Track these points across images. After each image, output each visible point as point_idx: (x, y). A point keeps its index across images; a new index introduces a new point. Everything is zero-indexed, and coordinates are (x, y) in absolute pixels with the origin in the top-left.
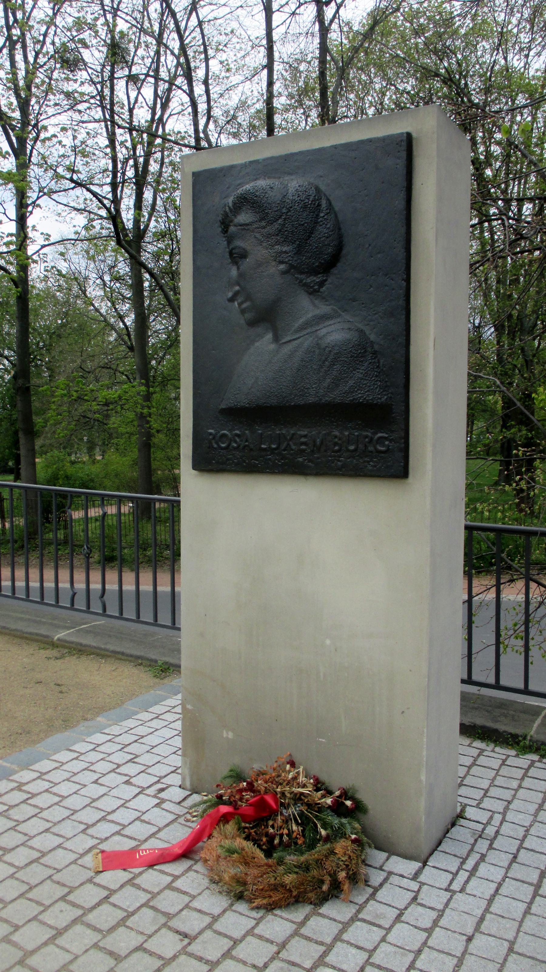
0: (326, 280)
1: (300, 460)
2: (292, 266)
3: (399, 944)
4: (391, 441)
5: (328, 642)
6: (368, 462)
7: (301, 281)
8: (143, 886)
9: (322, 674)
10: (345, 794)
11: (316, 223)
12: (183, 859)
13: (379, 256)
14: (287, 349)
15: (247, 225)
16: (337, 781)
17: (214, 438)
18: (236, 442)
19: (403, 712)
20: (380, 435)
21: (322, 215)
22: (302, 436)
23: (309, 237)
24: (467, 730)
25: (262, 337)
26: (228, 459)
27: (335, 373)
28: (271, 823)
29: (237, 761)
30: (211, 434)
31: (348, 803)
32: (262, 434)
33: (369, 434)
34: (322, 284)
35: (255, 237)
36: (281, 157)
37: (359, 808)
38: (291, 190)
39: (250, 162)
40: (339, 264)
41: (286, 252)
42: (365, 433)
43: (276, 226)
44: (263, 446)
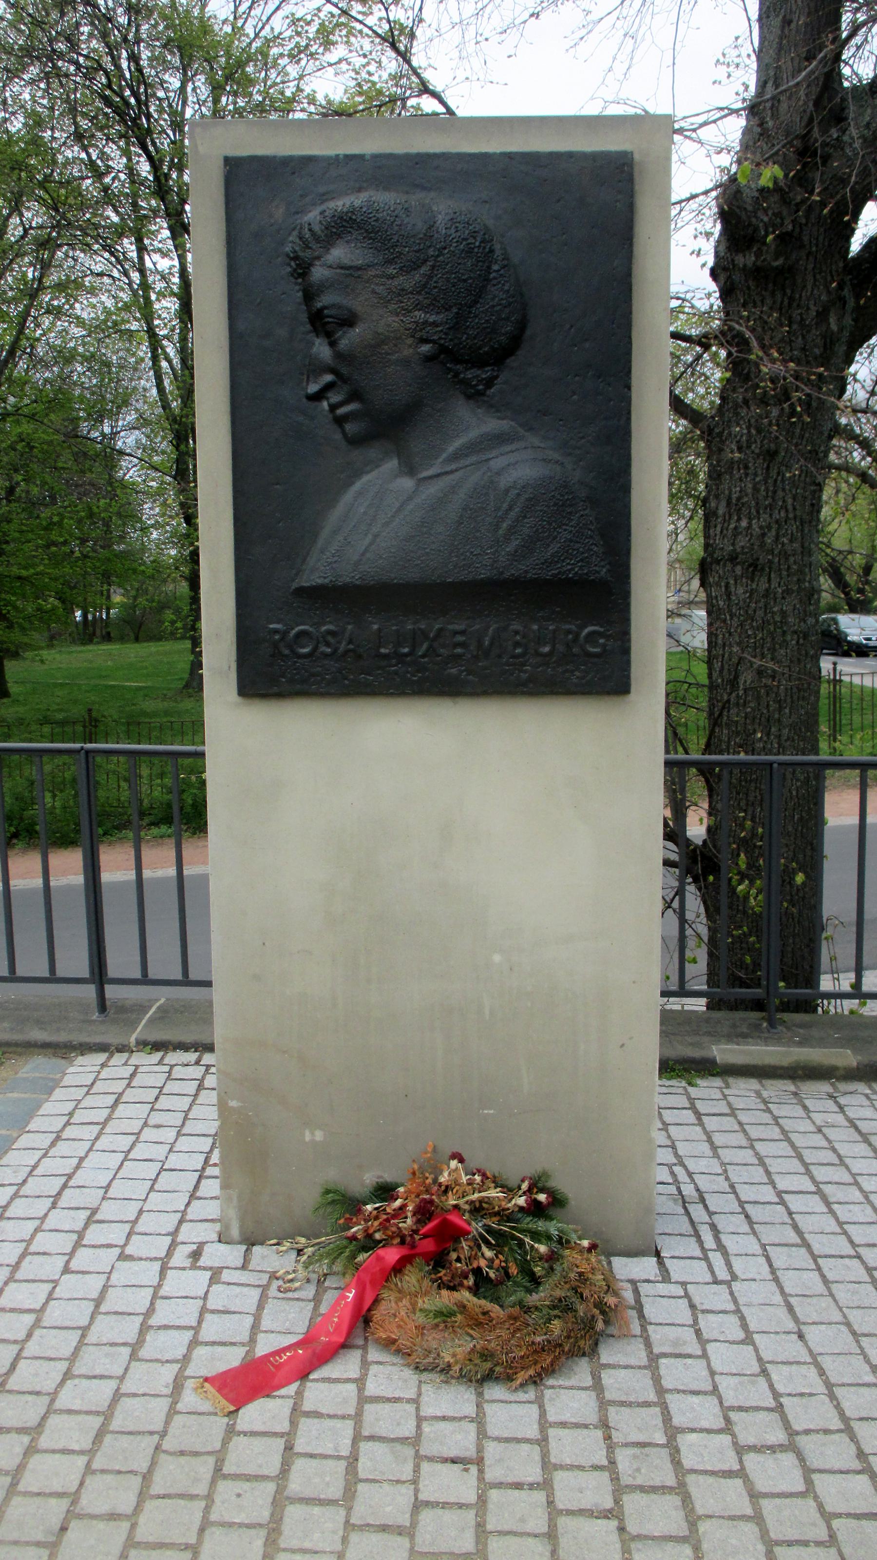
0: (497, 377)
1: (454, 671)
2: (443, 349)
3: (735, 1371)
4: (608, 637)
5: (497, 958)
6: (573, 671)
7: (456, 375)
8: (324, 1411)
9: (487, 1012)
10: (536, 1185)
11: (487, 280)
12: (341, 1351)
13: (587, 345)
14: (433, 489)
15: (358, 268)
16: (517, 1166)
17: (282, 639)
18: (328, 644)
19: (622, 1046)
20: (591, 628)
21: (495, 267)
22: (456, 633)
23: (476, 302)
25: (378, 466)
26: (313, 675)
27: (526, 531)
28: (454, 1256)
29: (332, 1174)
30: (276, 631)
32: (379, 630)
33: (573, 627)
34: (489, 383)
35: (374, 292)
36: (408, 157)
37: (557, 1201)
38: (441, 220)
39: (346, 156)
40: (519, 353)
41: (434, 324)
42: (567, 627)
43: (417, 277)
44: (383, 650)
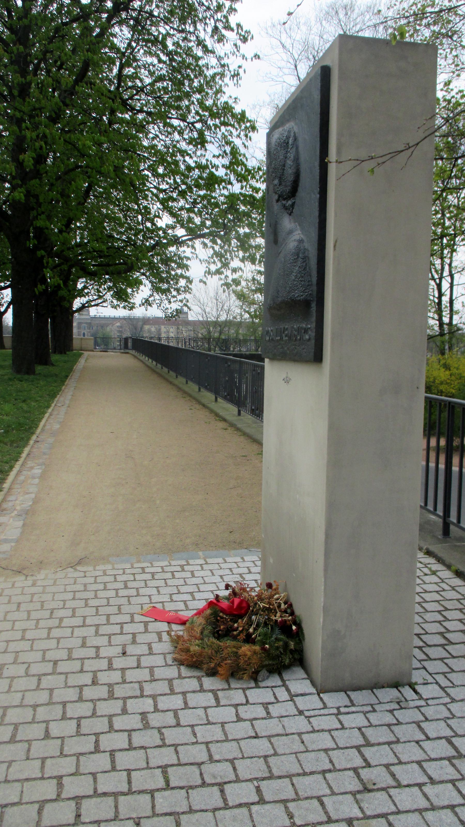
31: (294, 628)
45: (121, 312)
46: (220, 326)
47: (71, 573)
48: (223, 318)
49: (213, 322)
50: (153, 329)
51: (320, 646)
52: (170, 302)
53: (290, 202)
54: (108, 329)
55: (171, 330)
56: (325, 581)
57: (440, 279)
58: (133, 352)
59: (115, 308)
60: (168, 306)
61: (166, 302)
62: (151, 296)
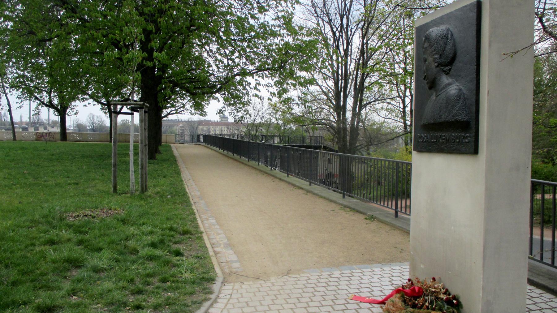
24: (531, 282)
31: (455, 301)
34: (450, 70)
45: (197, 117)
46: (256, 126)
47: (284, 279)
48: (258, 121)
49: (251, 124)
50: (205, 128)
51: (480, 310)
52: (237, 112)
53: (447, 68)
54: (174, 128)
55: (217, 129)
56: (483, 273)
57: (404, 97)
58: (204, 144)
59: (193, 114)
60: (236, 114)
61: (235, 111)
62: (224, 107)
